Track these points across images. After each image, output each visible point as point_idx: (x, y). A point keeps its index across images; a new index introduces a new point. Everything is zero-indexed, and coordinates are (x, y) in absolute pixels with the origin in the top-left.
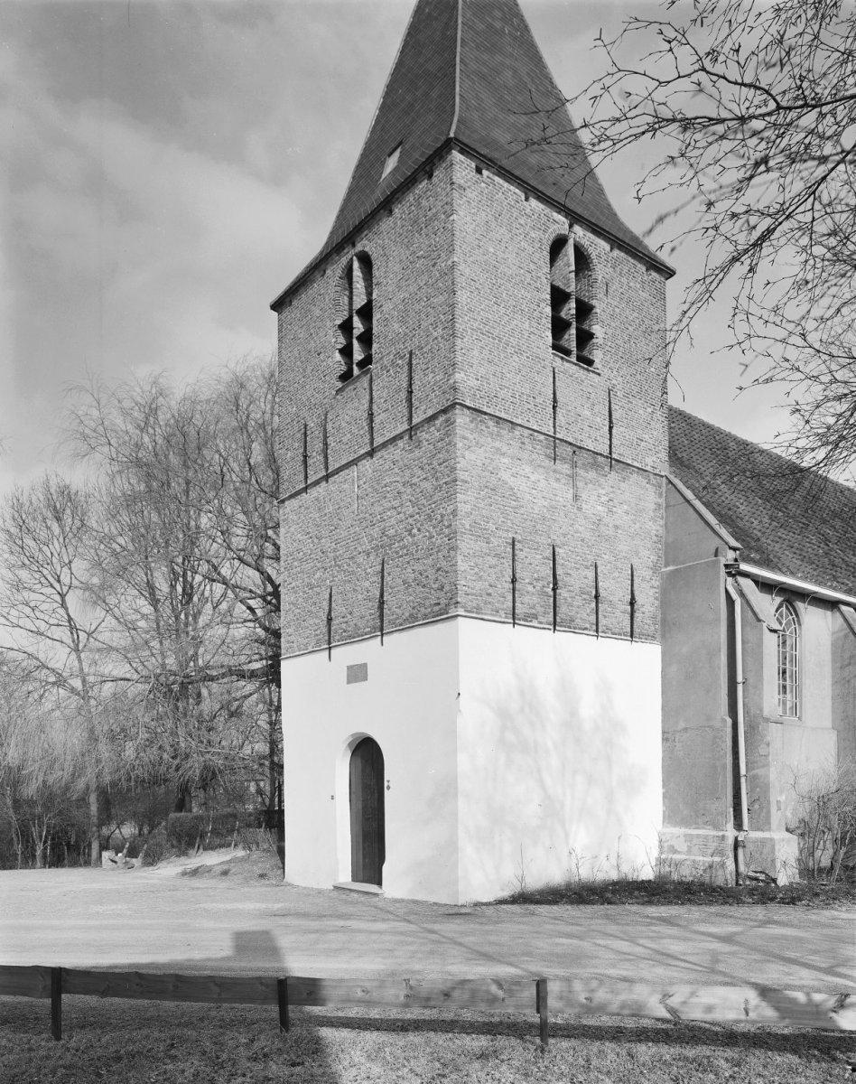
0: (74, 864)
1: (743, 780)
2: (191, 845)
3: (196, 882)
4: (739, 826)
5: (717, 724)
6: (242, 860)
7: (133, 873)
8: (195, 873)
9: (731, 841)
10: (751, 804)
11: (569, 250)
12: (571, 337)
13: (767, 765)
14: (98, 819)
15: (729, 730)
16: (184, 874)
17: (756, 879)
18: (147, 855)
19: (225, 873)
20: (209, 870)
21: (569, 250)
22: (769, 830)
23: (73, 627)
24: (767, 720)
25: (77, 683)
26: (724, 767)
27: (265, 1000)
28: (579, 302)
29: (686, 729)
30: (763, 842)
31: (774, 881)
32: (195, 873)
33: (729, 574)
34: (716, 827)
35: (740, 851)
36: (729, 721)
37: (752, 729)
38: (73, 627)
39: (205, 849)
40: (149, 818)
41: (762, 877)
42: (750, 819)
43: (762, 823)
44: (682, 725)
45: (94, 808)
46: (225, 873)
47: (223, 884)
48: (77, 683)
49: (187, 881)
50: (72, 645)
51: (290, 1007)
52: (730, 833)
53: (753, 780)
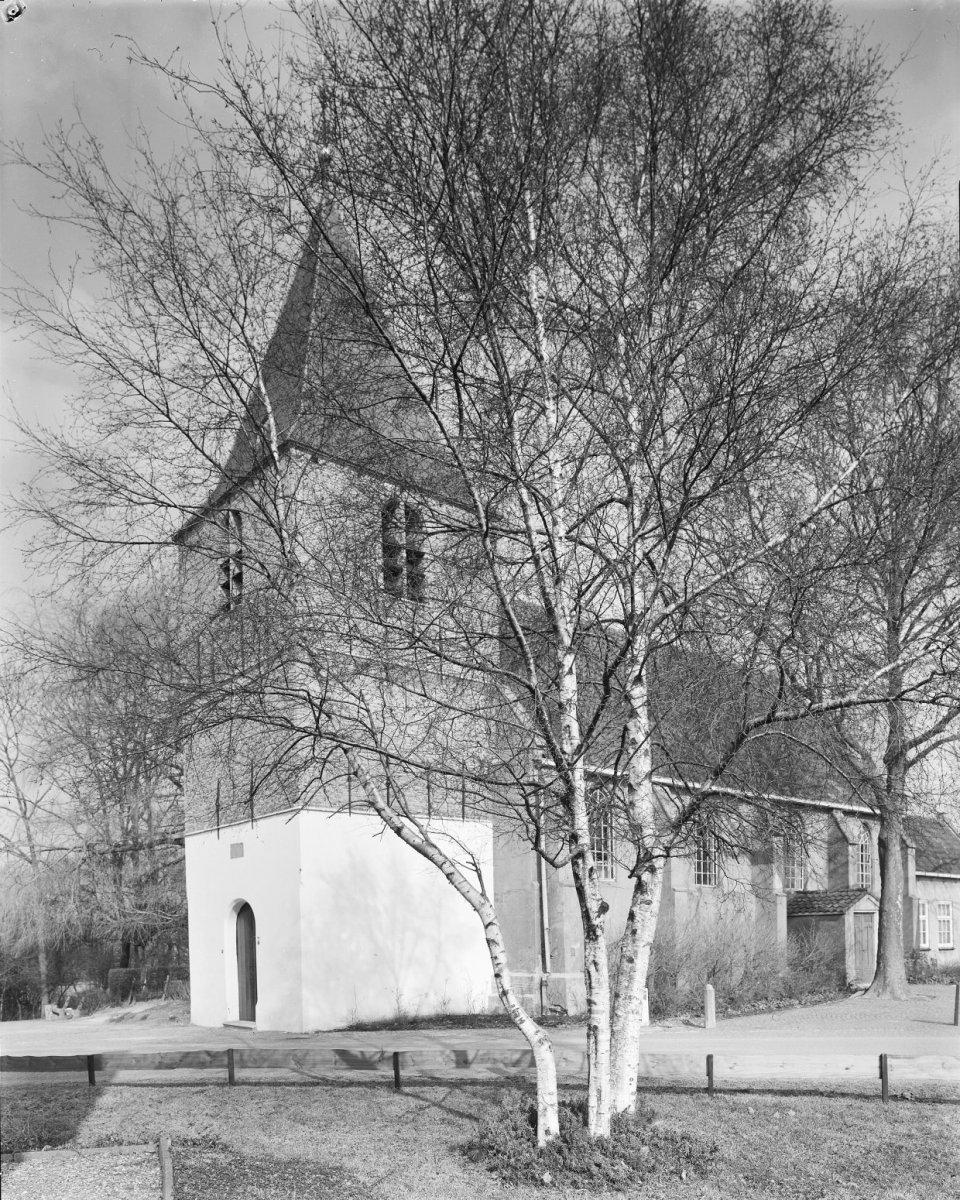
0: (29, 1017)
1: (546, 932)
2: (124, 997)
3: (120, 1027)
4: (544, 969)
5: (528, 887)
6: (163, 1008)
7: (71, 1022)
8: (121, 1019)
9: (537, 981)
10: (553, 951)
11: (400, 512)
12: (403, 581)
13: (562, 920)
14: (560, 665)
15: (537, 892)
16: (112, 1021)
17: (555, 1011)
18: (84, 1008)
19: (145, 1018)
20: (133, 1017)
21: (400, 512)
22: (564, 972)
23: (21, 800)
24: (561, 885)
25: (26, 850)
26: (533, 923)
27: (81, 1069)
28: (409, 553)
29: (509, 892)
30: (559, 981)
31: (566, 1011)
32: (121, 1019)
33: (536, 767)
34: (529, 970)
35: (544, 989)
36: (537, 884)
37: (552, 892)
38: (21, 800)
39: (137, 1001)
40: (100, 976)
41: (559, 1009)
42: (552, 963)
43: (559, 967)
44: (507, 888)
45: (43, 968)
46: (145, 1018)
47: (145, 1025)
48: (26, 850)
49: (113, 1026)
50: (20, 812)
51: (96, 1072)
52: (538, 974)
53: (552, 932)
